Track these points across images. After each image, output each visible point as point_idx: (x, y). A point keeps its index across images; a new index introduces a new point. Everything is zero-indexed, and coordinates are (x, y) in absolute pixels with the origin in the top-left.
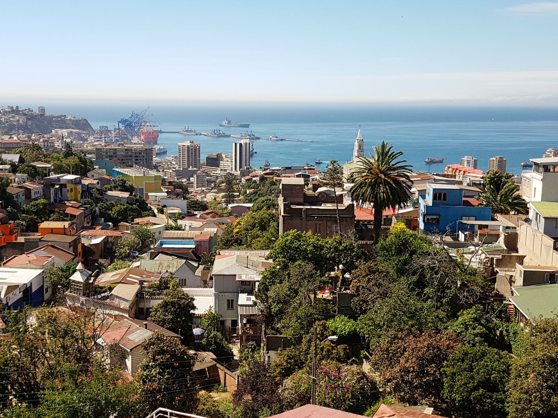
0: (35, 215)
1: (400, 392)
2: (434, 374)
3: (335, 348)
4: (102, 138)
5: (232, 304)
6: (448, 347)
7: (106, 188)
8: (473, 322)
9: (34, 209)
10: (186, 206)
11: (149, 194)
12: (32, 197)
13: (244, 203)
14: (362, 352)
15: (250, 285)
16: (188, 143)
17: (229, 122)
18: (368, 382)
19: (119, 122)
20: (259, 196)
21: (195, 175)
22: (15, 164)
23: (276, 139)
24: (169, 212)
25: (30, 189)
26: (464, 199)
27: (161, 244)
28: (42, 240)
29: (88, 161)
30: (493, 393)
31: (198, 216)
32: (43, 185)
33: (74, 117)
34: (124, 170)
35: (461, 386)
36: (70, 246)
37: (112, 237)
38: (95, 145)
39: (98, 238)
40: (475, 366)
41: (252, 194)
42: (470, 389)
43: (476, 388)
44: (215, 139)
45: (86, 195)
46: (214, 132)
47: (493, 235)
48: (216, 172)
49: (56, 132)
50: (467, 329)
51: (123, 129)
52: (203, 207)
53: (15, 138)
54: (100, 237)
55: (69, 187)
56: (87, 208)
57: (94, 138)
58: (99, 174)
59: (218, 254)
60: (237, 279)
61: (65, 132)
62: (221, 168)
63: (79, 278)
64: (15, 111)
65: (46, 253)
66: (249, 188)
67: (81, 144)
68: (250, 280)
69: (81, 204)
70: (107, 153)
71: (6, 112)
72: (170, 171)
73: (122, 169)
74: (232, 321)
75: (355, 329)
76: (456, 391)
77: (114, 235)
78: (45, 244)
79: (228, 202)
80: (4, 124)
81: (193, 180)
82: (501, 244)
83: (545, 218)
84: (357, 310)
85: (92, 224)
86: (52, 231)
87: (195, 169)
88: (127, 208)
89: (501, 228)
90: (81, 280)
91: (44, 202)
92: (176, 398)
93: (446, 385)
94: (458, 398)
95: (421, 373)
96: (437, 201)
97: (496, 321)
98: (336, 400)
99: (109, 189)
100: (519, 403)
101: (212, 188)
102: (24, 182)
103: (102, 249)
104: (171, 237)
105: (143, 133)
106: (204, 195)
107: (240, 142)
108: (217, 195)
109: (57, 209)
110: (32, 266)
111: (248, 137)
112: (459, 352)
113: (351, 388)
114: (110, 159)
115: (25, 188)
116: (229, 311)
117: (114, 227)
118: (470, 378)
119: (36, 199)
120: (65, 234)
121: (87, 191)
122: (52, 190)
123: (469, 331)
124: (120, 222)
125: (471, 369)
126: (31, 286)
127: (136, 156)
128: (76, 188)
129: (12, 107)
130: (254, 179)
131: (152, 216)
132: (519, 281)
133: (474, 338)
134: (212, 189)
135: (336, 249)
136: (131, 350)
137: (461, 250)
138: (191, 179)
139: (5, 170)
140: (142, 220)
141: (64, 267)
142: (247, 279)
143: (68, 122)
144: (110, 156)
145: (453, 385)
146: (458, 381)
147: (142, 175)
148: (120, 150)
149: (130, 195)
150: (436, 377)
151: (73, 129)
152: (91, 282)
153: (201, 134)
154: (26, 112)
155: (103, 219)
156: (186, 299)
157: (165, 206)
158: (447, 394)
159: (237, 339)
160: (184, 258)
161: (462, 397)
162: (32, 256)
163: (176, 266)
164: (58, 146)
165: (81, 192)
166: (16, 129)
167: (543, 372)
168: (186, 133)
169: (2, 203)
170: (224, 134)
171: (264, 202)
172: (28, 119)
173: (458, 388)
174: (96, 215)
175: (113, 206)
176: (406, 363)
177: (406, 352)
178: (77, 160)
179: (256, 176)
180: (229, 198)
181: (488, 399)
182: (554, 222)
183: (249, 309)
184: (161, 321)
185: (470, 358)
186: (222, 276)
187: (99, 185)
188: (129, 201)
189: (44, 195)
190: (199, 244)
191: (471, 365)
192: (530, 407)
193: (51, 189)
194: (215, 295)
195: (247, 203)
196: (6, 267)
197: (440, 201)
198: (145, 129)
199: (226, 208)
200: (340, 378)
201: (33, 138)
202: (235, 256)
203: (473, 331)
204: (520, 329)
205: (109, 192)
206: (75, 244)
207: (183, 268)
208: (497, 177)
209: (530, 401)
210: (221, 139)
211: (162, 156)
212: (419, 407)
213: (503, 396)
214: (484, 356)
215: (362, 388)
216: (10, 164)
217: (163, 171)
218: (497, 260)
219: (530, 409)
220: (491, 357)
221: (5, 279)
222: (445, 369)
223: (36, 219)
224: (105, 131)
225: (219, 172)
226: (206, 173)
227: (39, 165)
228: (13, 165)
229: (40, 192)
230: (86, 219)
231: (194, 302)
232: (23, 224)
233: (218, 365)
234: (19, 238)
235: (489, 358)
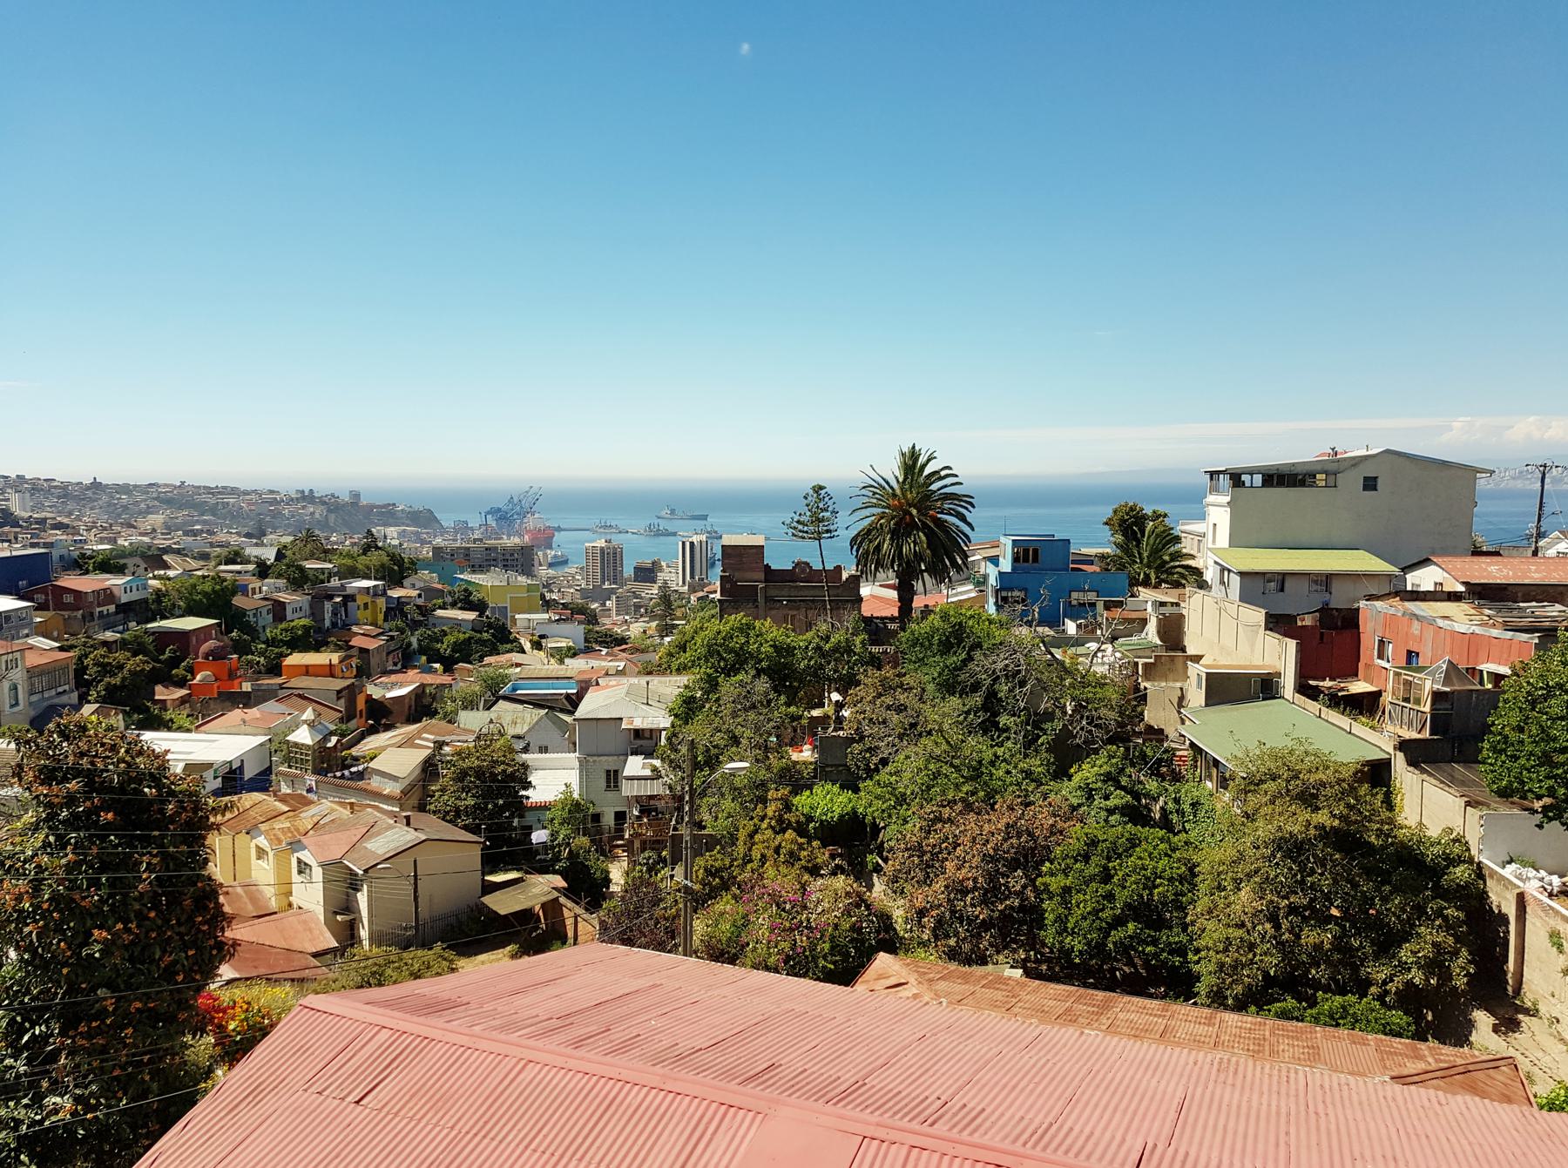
1: (947, 937)
2: (1019, 894)
3: (805, 846)
5: (613, 778)
6: (1053, 830)
7: (435, 605)
8: (1104, 782)
11: (517, 616)
14: (869, 858)
15: (651, 738)
16: (601, 543)
17: (673, 512)
18: (869, 915)
22: (265, 563)
24: (549, 645)
25: (284, 603)
26: (1071, 566)
27: (515, 689)
30: (1160, 931)
31: (603, 653)
32: (310, 597)
35: (1084, 918)
36: (338, 698)
39: (405, 686)
40: (1116, 870)
42: (1107, 923)
43: (1119, 922)
44: (648, 538)
47: (1132, 621)
50: (1090, 797)
55: (361, 600)
56: (392, 638)
58: (425, 581)
59: (594, 683)
60: (623, 727)
63: (306, 737)
64: (307, 497)
67: (416, 548)
68: (650, 726)
70: (452, 555)
71: (292, 500)
72: (572, 590)
75: (853, 809)
76: (1073, 929)
82: (1150, 636)
83: (1241, 574)
84: (859, 770)
86: (307, 671)
89: (1150, 603)
90: (309, 742)
92: (96, 932)
93: (1049, 917)
94: (1077, 944)
95: (992, 892)
96: (1022, 564)
97: (1152, 785)
98: (794, 959)
100: (1226, 950)
101: (642, 616)
103: (410, 707)
110: (248, 729)
112: (1078, 839)
113: (830, 929)
116: (610, 795)
117: (445, 672)
118: (1104, 897)
120: (332, 676)
121: (396, 609)
122: (328, 606)
123: (1096, 802)
124: (457, 664)
125: (1106, 876)
126: (241, 768)
129: (303, 492)
130: (712, 596)
131: (518, 652)
132: (1196, 696)
133: (1108, 817)
135: (818, 648)
136: (366, 871)
137: (1072, 651)
138: (608, 602)
142: (645, 726)
143: (400, 514)
145: (1066, 917)
146: (1078, 907)
147: (505, 584)
149: (480, 616)
150: (1027, 899)
152: (329, 745)
154: (326, 499)
156: (507, 764)
157: (542, 637)
158: (1054, 938)
159: (624, 851)
161: (1088, 944)
162: (254, 712)
163: (528, 720)
167: (1277, 876)
168: (602, 530)
169: (221, 623)
172: (329, 511)
173: (1077, 922)
175: (445, 634)
176: (958, 869)
177: (959, 845)
178: (386, 559)
181: (1148, 945)
182: (1259, 583)
183: (646, 785)
184: (451, 811)
185: (1103, 851)
188: (476, 627)
191: (1106, 868)
192: (1251, 960)
196: (201, 732)
197: (1026, 564)
200: (805, 907)
201: (333, 539)
203: (1104, 803)
204: (1206, 794)
206: (350, 694)
208: (1134, 517)
209: (1252, 947)
211: (560, 568)
212: (990, 967)
213: (1184, 938)
214: (1134, 846)
215: (855, 928)
217: (559, 591)
218: (1145, 665)
219: (1252, 963)
220: (1150, 849)
222: (1047, 879)
224: (463, 528)
226: (634, 592)
229: (303, 609)
232: (259, 662)
233: (563, 900)
234: (244, 684)
235: (1146, 850)
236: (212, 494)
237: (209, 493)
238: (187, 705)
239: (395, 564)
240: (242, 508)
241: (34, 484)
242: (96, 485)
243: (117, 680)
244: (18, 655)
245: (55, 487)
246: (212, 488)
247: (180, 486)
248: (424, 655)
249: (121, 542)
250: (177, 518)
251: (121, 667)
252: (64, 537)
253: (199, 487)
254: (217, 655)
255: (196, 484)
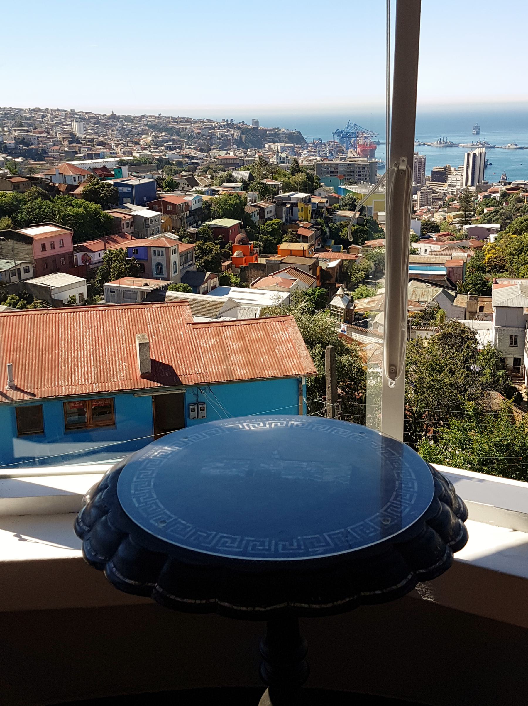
0: (270, 236)
4: (315, 152)
7: (335, 207)
9: (269, 229)
10: (420, 227)
11: (379, 214)
12: (266, 217)
13: (481, 224)
19: (334, 134)
20: (501, 215)
21: (419, 192)
23: (515, 147)
25: (264, 208)
28: (282, 261)
29: (315, 178)
32: (275, 204)
33: (288, 130)
34: (351, 187)
36: (310, 269)
37: (346, 260)
38: (310, 160)
39: (333, 261)
41: (492, 213)
44: (438, 149)
45: (316, 214)
46: (440, 142)
48: (442, 188)
49: (269, 146)
51: (337, 141)
52: (436, 228)
53: (232, 154)
54: (335, 260)
57: (308, 152)
58: (327, 191)
60: (524, 313)
61: (276, 146)
62: (449, 183)
64: (230, 125)
65: (289, 275)
66: (487, 206)
69: (312, 224)
73: (349, 187)
74: (515, 359)
77: (348, 258)
78: (285, 266)
79: (463, 223)
80: (219, 138)
81: (416, 198)
85: (323, 247)
86: (292, 253)
87: (419, 185)
88: (358, 229)
91: (278, 222)
99: (338, 208)
101: (440, 207)
102: (255, 201)
104: (417, 262)
105: (360, 146)
106: (431, 215)
107: (474, 152)
108: (447, 215)
109: (289, 230)
110: (279, 288)
111: (480, 145)
114: (331, 176)
115: (259, 207)
116: (512, 348)
119: (270, 219)
120: (304, 256)
121: (317, 211)
122: (284, 209)
124: (351, 245)
127: (358, 172)
128: (307, 208)
134: (439, 208)
139: (237, 188)
140: (374, 243)
141: (310, 291)
143: (281, 135)
144: (331, 172)
148: (342, 165)
151: (286, 143)
153: (424, 144)
155: (333, 241)
160: (440, 286)
162: (278, 278)
163: (431, 294)
164: (273, 161)
165: (311, 212)
166: (232, 144)
170: (452, 142)
171: (522, 223)
172: (242, 133)
174: (326, 236)
179: (496, 192)
180: (466, 217)
186: (506, 309)
187: (328, 204)
189: (276, 214)
190: (451, 271)
193: (283, 208)
194: (496, 329)
195: (485, 223)
198: (361, 141)
199: (460, 229)
201: (248, 153)
202: (518, 286)
205: (340, 211)
207: (440, 296)
210: (448, 149)
216: (242, 182)
221: (256, 300)
223: (271, 239)
224: (318, 144)
225: (446, 188)
226: (431, 189)
227: (269, 182)
228: (244, 182)
229: (272, 211)
230: (317, 240)
231: (477, 336)
234: (259, 259)
236: (177, 122)
237: (175, 122)
238: (231, 268)
239: (309, 181)
240: (193, 131)
241: (80, 115)
242: (114, 117)
243: (209, 258)
244: (176, 247)
245: (92, 117)
246: (176, 119)
247: (158, 117)
248: (333, 239)
249: (134, 154)
250: (158, 137)
251: (211, 251)
252: (105, 150)
253: (169, 118)
254: (243, 242)
255: (167, 116)
